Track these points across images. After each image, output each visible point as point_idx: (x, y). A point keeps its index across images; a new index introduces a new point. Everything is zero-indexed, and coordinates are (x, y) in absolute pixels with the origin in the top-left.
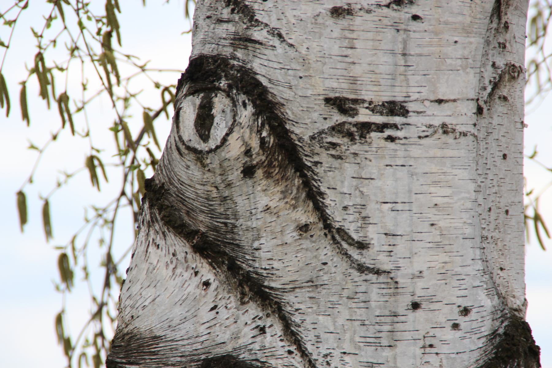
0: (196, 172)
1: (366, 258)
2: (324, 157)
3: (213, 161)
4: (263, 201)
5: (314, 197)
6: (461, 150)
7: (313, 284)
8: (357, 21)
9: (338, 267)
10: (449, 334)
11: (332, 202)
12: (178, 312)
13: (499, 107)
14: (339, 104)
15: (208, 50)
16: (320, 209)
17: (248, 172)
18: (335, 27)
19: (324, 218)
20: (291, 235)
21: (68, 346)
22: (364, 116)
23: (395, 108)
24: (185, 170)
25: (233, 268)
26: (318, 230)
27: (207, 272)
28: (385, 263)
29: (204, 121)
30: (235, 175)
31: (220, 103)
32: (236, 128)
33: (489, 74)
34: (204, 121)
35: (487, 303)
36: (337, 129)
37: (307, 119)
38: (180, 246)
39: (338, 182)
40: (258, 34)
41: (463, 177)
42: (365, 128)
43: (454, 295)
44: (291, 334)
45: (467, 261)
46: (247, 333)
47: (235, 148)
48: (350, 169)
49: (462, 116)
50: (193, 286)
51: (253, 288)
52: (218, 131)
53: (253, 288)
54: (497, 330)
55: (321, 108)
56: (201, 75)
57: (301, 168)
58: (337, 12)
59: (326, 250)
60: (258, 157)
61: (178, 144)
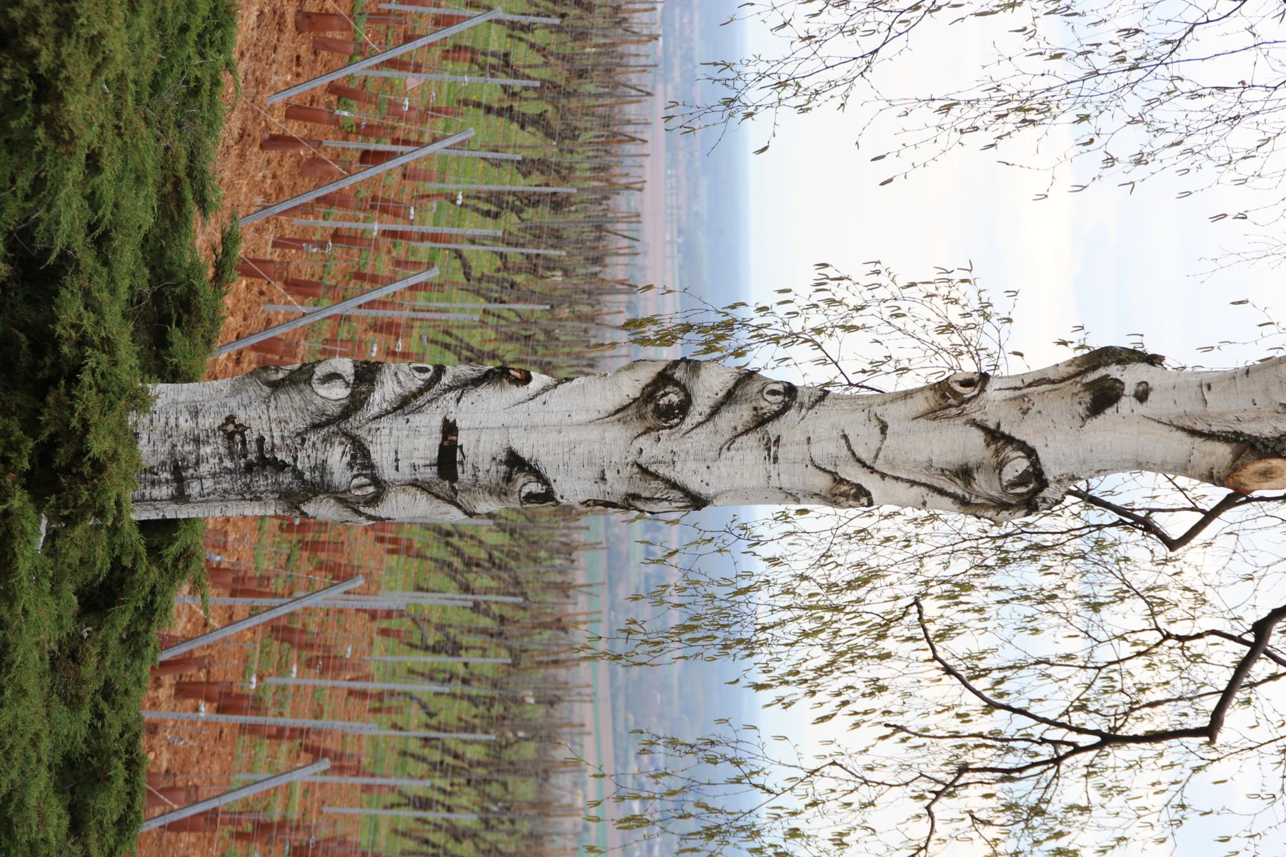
0: (756, 390)
1: (724, 450)
2: (760, 435)
3: (759, 396)
4: (745, 414)
5: (746, 432)
6: (763, 482)
7: (716, 432)
8: (806, 446)
9: (722, 441)
10: (699, 479)
11: (744, 438)
12: (707, 384)
13: (783, 496)
14: (778, 440)
15: (799, 393)
16: (742, 434)
17: (755, 409)
18: (804, 438)
19: (739, 435)
20: (733, 424)
21: (734, 307)
22: (773, 449)
23: (776, 459)
24: (480, 598)
25: (722, 404)
26: (735, 433)
27: (721, 394)
28: (723, 457)
29: (774, 393)
30: (754, 404)
31: (780, 398)
32: (771, 404)
33: (794, 492)
34: (774, 393)
35: (711, 492)
36: (769, 440)
37: (773, 429)
38: (730, 385)
39: (751, 440)
40: (804, 411)
41: (753, 483)
42: (769, 449)
43: (712, 481)
44: (699, 424)
45: (724, 486)
46: (699, 409)
47: (763, 404)
48: (755, 444)
49: (775, 482)
50: (716, 389)
51: (715, 411)
52: (770, 398)
53: (715, 411)
54: (450, 626)
55: (777, 434)
56: (790, 390)
57: (756, 427)
58: (809, 439)
59: (728, 436)
60: (760, 412)
61: (766, 382)
